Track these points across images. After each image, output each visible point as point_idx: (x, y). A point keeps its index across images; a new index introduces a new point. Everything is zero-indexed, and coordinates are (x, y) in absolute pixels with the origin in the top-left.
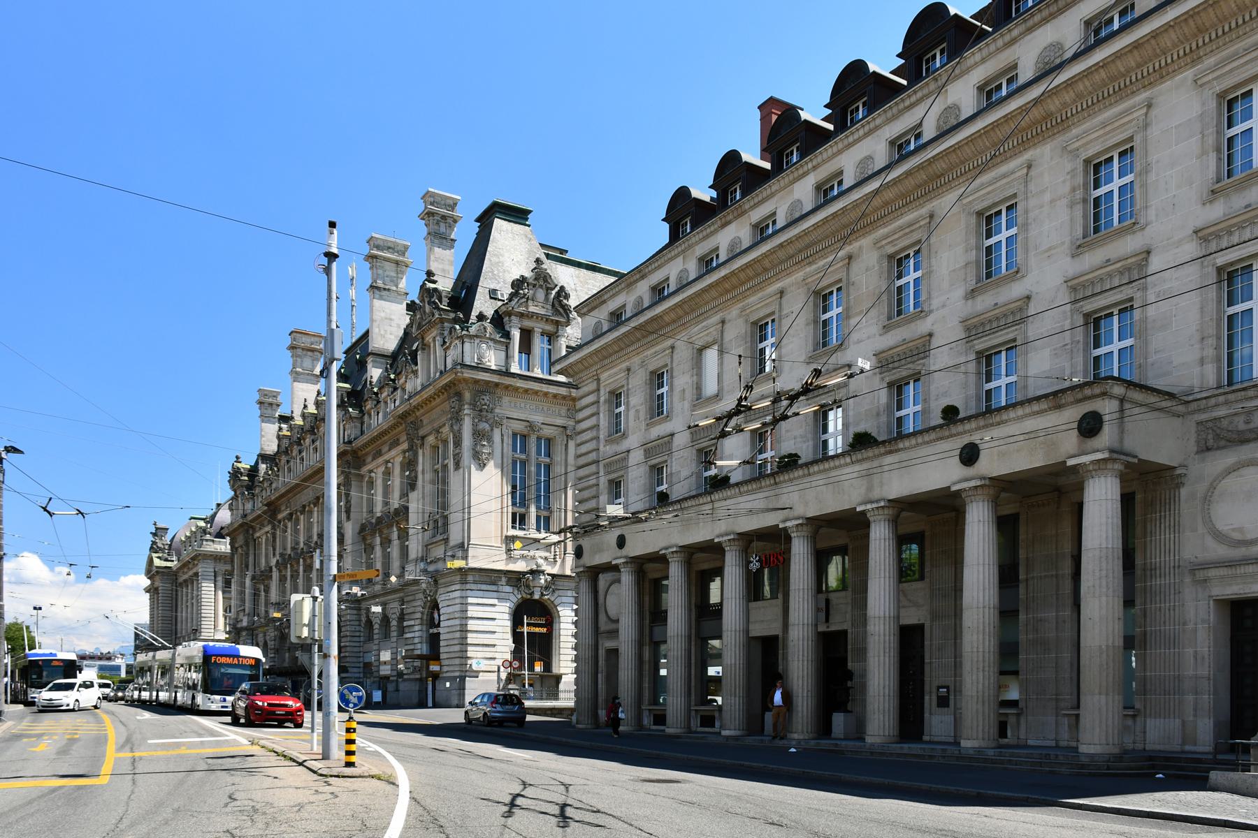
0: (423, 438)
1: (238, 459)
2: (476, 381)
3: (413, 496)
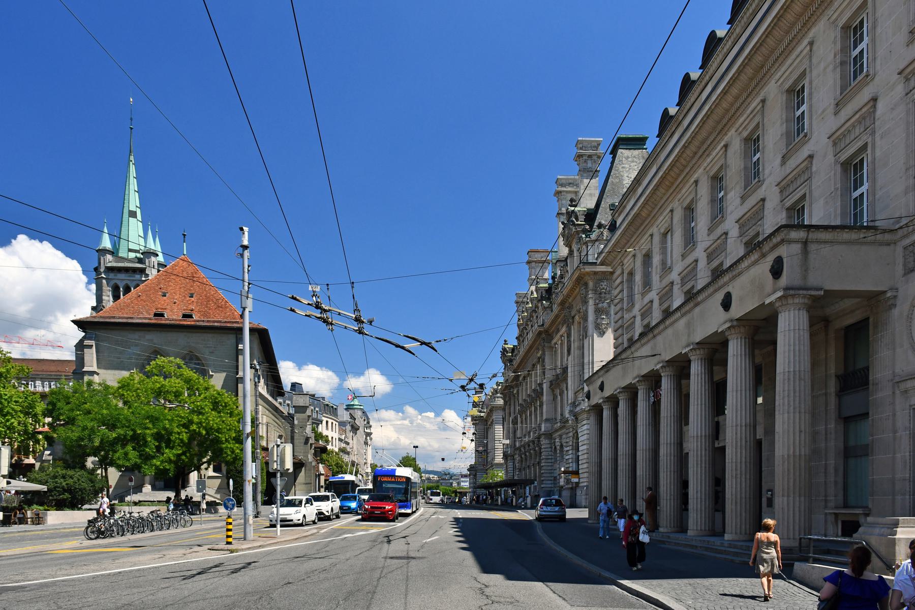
0: (573, 317)
1: (506, 342)
2: (595, 273)
3: (570, 358)
